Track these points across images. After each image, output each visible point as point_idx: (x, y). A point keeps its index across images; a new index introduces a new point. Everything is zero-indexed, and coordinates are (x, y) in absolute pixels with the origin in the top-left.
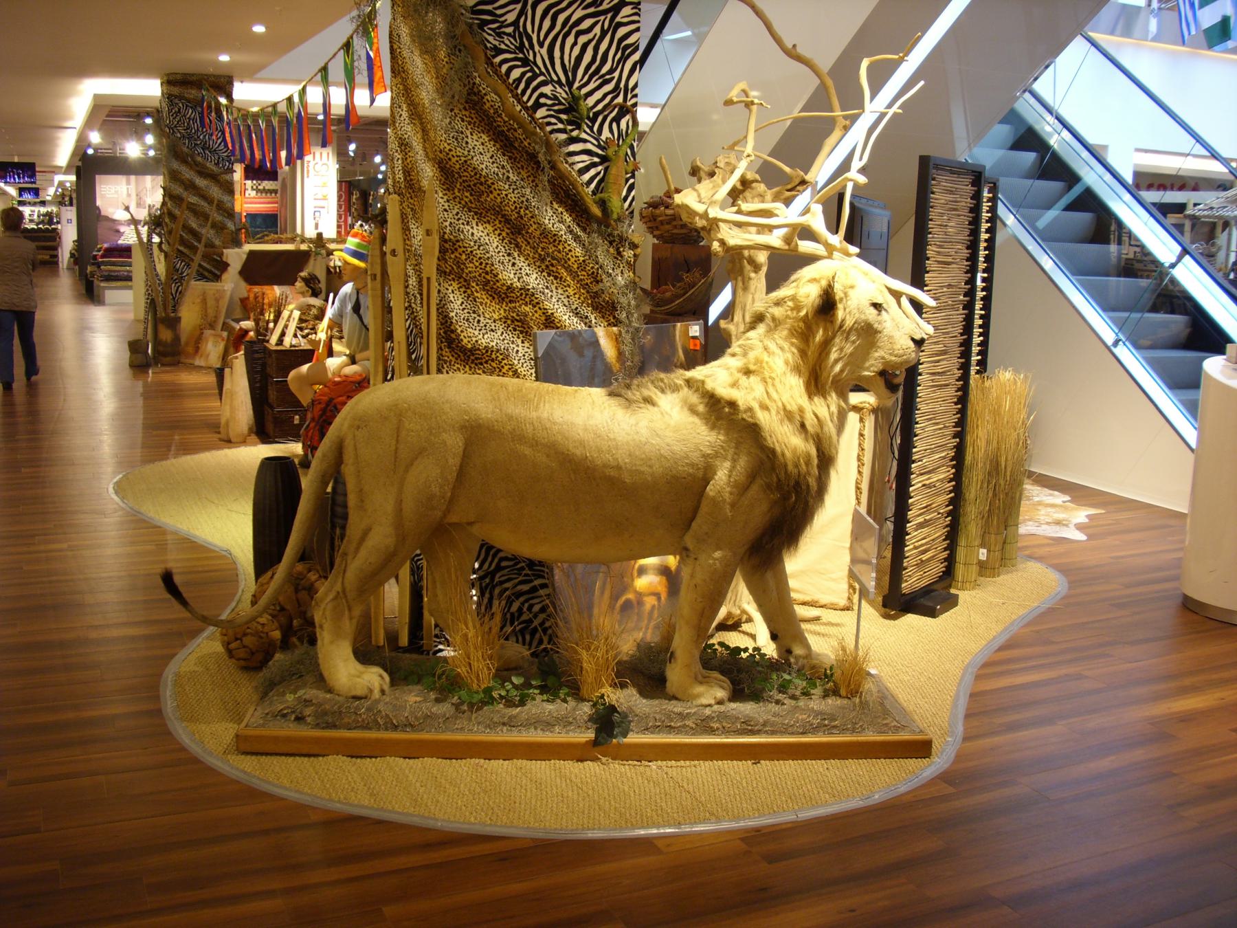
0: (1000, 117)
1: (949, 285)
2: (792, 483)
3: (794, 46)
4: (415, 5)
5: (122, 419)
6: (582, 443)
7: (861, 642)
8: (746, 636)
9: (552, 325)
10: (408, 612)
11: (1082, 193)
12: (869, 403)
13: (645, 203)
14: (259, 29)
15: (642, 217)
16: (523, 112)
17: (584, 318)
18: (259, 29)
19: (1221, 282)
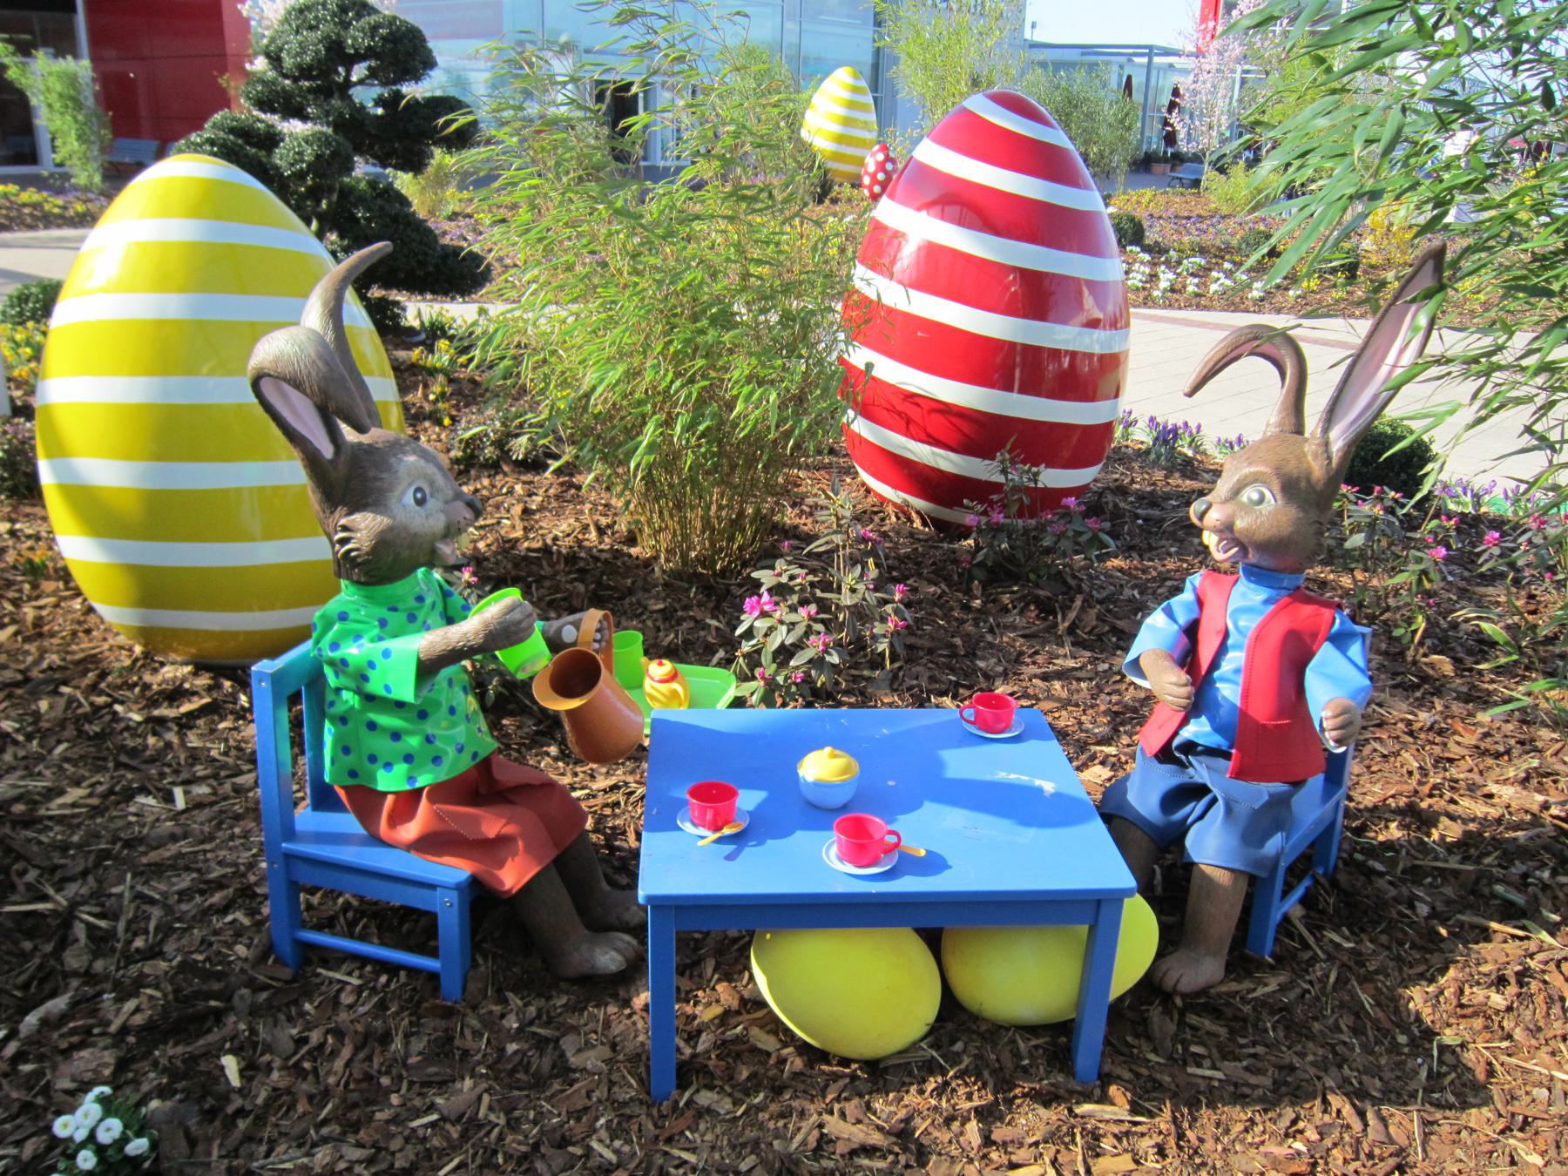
0: (677, 833)
1: (515, 184)
2: (1412, 1018)
3: (1199, 427)
4: (922, 1155)
5: (496, 601)
6: (1269, 534)
7: (547, 25)
8: (296, 453)
9: (815, 563)
10: (1002, 776)
11: (116, 195)
12: (1527, 812)
13: (1199, 427)
14: (891, 783)
15: (378, 176)
16: (1469, 509)
17: (280, 1107)
18: (891, 783)
19: (338, 874)
